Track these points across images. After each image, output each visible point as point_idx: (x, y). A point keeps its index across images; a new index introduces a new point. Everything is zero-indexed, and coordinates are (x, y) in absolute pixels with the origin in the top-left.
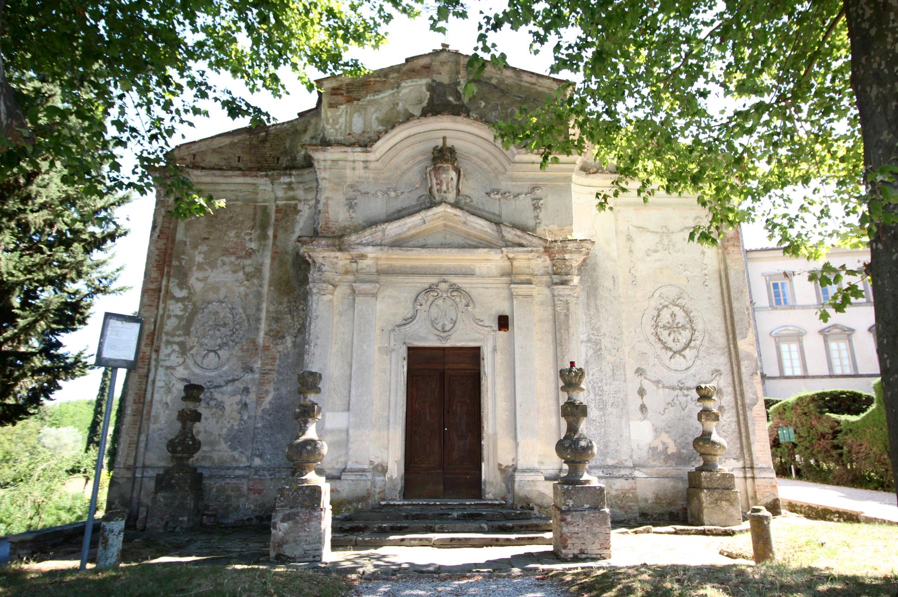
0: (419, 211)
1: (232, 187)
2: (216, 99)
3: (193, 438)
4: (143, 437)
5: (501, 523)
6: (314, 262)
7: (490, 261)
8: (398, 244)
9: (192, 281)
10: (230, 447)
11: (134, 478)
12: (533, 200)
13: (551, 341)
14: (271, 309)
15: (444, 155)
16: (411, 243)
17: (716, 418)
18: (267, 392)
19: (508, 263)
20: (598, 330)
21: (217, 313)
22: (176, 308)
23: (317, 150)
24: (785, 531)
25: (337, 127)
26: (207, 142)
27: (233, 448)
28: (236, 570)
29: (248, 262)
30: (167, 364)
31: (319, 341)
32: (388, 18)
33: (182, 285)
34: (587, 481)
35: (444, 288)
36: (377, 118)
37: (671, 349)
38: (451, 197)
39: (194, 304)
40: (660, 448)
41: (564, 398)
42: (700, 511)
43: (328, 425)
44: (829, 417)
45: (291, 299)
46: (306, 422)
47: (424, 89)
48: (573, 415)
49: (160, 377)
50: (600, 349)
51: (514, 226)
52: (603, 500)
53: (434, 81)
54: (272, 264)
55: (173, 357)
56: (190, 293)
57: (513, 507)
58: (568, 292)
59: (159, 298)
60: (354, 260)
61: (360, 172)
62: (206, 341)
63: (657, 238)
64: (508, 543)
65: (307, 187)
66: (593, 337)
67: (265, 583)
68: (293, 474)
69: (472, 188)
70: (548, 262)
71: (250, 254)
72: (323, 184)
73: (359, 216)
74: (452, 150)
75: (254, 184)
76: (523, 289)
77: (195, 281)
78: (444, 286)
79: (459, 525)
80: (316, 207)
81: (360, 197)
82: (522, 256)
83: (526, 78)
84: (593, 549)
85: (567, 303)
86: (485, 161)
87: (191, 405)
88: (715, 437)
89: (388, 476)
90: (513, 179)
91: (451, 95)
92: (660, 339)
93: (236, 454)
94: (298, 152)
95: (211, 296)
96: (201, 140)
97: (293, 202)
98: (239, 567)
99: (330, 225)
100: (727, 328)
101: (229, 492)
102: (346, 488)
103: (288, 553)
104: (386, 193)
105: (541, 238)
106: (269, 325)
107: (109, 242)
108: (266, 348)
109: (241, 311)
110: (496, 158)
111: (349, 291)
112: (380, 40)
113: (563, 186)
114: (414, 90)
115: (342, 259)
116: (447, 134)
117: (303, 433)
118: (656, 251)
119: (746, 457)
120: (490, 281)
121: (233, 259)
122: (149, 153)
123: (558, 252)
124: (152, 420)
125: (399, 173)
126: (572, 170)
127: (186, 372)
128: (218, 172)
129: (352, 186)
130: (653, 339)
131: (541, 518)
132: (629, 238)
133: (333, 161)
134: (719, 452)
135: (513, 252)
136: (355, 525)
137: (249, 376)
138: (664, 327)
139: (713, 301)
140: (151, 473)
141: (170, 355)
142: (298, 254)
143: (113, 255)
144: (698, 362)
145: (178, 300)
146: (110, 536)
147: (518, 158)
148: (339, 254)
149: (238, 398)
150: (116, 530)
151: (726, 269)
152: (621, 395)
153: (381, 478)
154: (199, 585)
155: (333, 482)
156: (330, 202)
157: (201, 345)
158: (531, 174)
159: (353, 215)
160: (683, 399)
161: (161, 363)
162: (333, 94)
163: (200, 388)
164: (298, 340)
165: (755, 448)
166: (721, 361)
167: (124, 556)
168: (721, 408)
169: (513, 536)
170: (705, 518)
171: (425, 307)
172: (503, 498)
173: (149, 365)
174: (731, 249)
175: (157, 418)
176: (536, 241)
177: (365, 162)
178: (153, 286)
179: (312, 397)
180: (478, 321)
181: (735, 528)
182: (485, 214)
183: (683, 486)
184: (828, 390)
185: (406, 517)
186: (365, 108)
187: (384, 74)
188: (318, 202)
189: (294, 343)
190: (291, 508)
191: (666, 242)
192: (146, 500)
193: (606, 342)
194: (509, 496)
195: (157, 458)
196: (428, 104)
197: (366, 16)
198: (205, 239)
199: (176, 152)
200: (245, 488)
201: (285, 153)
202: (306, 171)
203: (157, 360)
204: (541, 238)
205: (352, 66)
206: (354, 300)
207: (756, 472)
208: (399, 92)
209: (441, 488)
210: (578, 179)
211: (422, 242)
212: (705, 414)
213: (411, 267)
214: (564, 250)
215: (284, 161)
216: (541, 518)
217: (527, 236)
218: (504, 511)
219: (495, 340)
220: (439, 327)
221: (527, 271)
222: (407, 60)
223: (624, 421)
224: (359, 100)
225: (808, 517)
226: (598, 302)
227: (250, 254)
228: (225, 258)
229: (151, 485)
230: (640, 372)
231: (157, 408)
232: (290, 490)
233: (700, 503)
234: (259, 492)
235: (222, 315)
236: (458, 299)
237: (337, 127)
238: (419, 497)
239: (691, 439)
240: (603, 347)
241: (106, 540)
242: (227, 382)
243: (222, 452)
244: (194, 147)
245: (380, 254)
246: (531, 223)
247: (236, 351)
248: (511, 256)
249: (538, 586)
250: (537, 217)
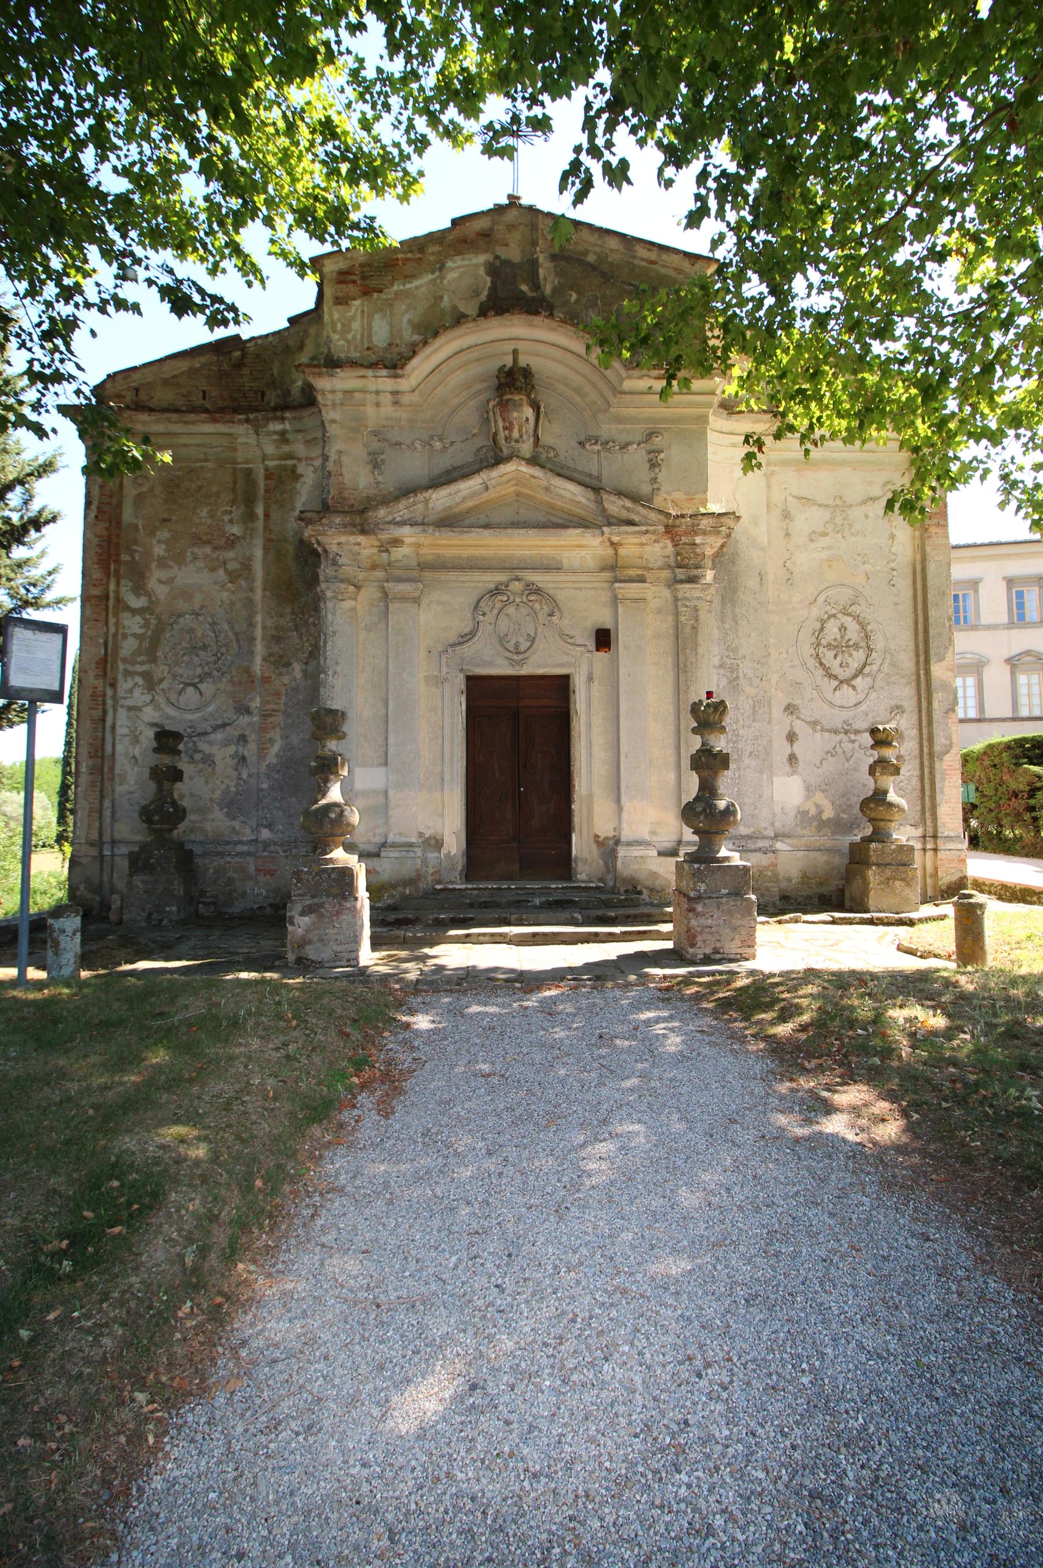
0: (478, 471)
1: (198, 440)
2: (150, 282)
3: (174, 803)
4: (107, 803)
5: (600, 913)
6: (326, 551)
7: (583, 548)
8: (449, 522)
9: (152, 584)
10: (227, 815)
11: (102, 857)
12: (649, 452)
13: (670, 665)
14: (269, 623)
15: (515, 380)
16: (467, 522)
17: (897, 771)
18: (271, 741)
19: (610, 551)
20: (735, 650)
21: (192, 631)
22: (133, 624)
23: (320, 375)
24: (999, 919)
25: (350, 336)
26: (153, 369)
27: (231, 816)
28: (238, 980)
29: (231, 554)
30: (129, 702)
31: (339, 668)
32: (421, 144)
33: (139, 589)
34: (727, 859)
35: (518, 588)
36: (410, 321)
37: (836, 677)
38: (526, 448)
40: (813, 811)
41: (696, 743)
42: (865, 892)
43: (359, 785)
44: (1026, 771)
46: (326, 781)
47: (482, 271)
48: (709, 767)
49: (123, 721)
51: (620, 494)
52: (747, 883)
53: (497, 257)
54: (265, 558)
55: (137, 693)
56: (150, 601)
57: (614, 890)
58: (696, 594)
59: (107, 609)
60: (384, 548)
61: (388, 410)
62: (180, 671)
63: (827, 515)
64: (611, 938)
67: (279, 1003)
68: (315, 849)
69: (557, 435)
70: (670, 549)
71: (232, 542)
72: (333, 430)
73: (389, 480)
74: (527, 373)
75: (230, 435)
76: (632, 590)
77: (156, 581)
78: (516, 586)
79: (543, 916)
80: (323, 467)
82: (632, 540)
83: (641, 252)
84: (732, 947)
85: (696, 609)
86: (577, 391)
87: (167, 760)
88: (892, 797)
89: (444, 851)
90: (619, 420)
91: (524, 281)
93: (236, 824)
94: (293, 382)
95: (181, 605)
96: (145, 365)
98: (244, 975)
99: (346, 494)
100: (917, 646)
101: (231, 874)
102: (388, 867)
103: (312, 956)
104: (428, 443)
105: (661, 512)
106: (268, 647)
107: (32, 532)
108: (265, 680)
109: (226, 626)
110: (594, 385)
111: (379, 595)
112: (410, 184)
113: (694, 433)
114: (466, 272)
115: (366, 546)
116: (521, 346)
117: (324, 795)
118: (824, 534)
119: (929, 823)
120: (583, 577)
121: (208, 550)
122: (43, 366)
123: (686, 534)
125: (447, 410)
126: (709, 405)
127: (157, 714)
128: (174, 416)
129: (375, 433)
130: (812, 663)
131: (652, 905)
132: (786, 515)
133: (345, 392)
134: (897, 817)
135: (619, 534)
136: (406, 916)
137: (244, 720)
138: (829, 646)
139: (901, 607)
140: (124, 850)
141: (131, 690)
142: (302, 542)
143: (43, 554)
144: (873, 695)
145: (134, 612)
146: (62, 937)
147: (628, 385)
148: (361, 539)
149: (232, 749)
150: (69, 930)
151: (924, 560)
154: (186, 1007)
155: (369, 861)
156: (344, 459)
157: (175, 676)
158: (647, 412)
159: (380, 479)
160: (847, 746)
162: (340, 282)
163: (177, 736)
164: (310, 668)
165: (943, 811)
166: (905, 694)
167: (86, 960)
168: (899, 758)
169: (617, 930)
170: (872, 903)
171: (490, 618)
172: (601, 880)
173: (104, 704)
174: (933, 530)
175: (123, 778)
176: (653, 516)
177: (395, 393)
178: (96, 592)
179: (332, 745)
180: (565, 637)
181: (914, 915)
182: (576, 475)
183: (840, 861)
184: (1030, 735)
185: (471, 905)
186: (391, 306)
187: (417, 246)
188: (326, 458)
189: (305, 672)
190: (313, 897)
191: (839, 520)
192: (120, 885)
193: (746, 668)
194: (609, 877)
195: (129, 831)
196: (489, 296)
197: (386, 140)
198: (165, 520)
199: (108, 386)
200: (252, 868)
201: (273, 384)
202: (306, 413)
203: (114, 698)
204: (661, 512)
205: (364, 230)
206: (387, 607)
207: (940, 842)
208: (442, 278)
209: (517, 866)
210: (717, 422)
211: (483, 520)
212: (880, 767)
213: (469, 559)
214: (694, 531)
215: (273, 397)
216: (652, 905)
217: (641, 509)
218: (603, 897)
220: (511, 646)
221: (639, 562)
222: (455, 222)
224: (380, 291)
225: (1000, 898)
227: (232, 542)
228: (196, 550)
229: (124, 864)
230: (790, 709)
231: (122, 764)
232: (309, 873)
233: (866, 883)
234: (272, 873)
235: (199, 634)
236: (537, 606)
237: (350, 336)
238: (487, 879)
239: (856, 801)
241: (56, 944)
242: (216, 728)
243: (218, 821)
244: (135, 376)
245: (422, 539)
246: (645, 489)
247: (224, 684)
248: (615, 539)
249: (663, 1000)
250: (654, 480)
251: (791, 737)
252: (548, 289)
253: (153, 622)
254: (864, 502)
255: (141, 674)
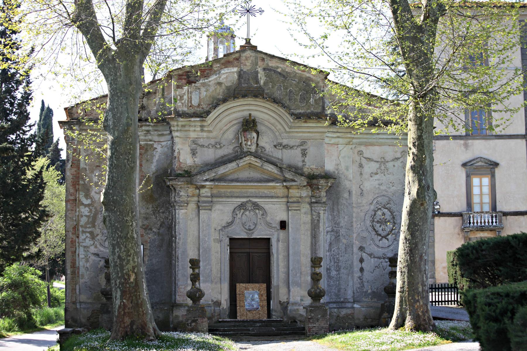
8: (221, 179)
12: (302, 150)
25: (183, 101)
30: (84, 244)
33: (87, 196)
39: (96, 208)
45: (154, 206)
49: (81, 252)
50: (339, 236)
55: (87, 240)
65: (160, 133)
66: (335, 229)
81: (198, 148)
92: (374, 229)
97: (151, 143)
99: (182, 165)
118: (377, 174)
124: (80, 277)
125: (222, 132)
127: (96, 250)
130: (370, 229)
138: (378, 222)
145: (86, 206)
152: (350, 262)
153: (218, 308)
157: (103, 234)
161: (81, 244)
175: (83, 275)
178: (72, 198)
191: (383, 168)
193: (342, 232)
198: (97, 166)
219: (278, 235)
223: (350, 277)
224: (195, 83)
226: (339, 207)
230: (361, 249)
231: (82, 270)
240: (341, 234)
250: (303, 161)
251: (361, 260)
252: (262, 82)
253: (93, 210)
254: (393, 160)
255: (89, 232)
